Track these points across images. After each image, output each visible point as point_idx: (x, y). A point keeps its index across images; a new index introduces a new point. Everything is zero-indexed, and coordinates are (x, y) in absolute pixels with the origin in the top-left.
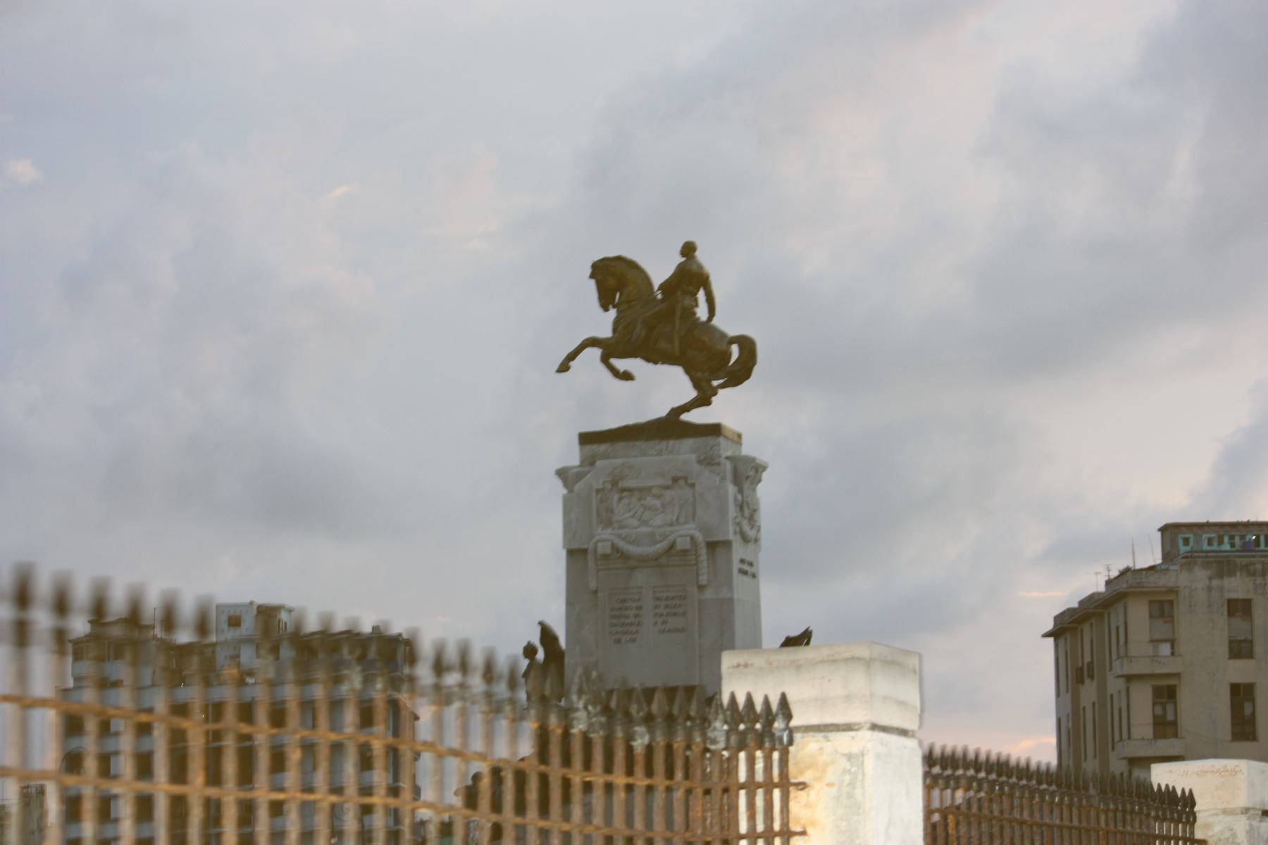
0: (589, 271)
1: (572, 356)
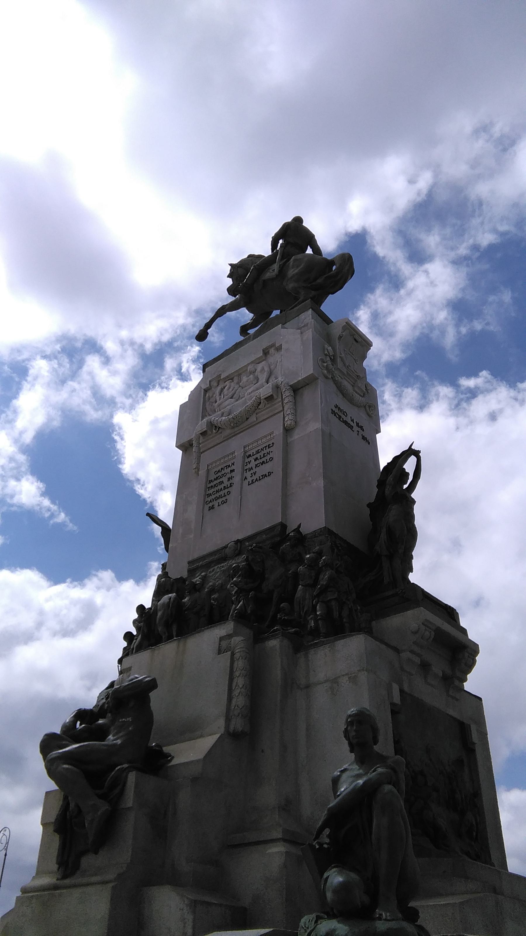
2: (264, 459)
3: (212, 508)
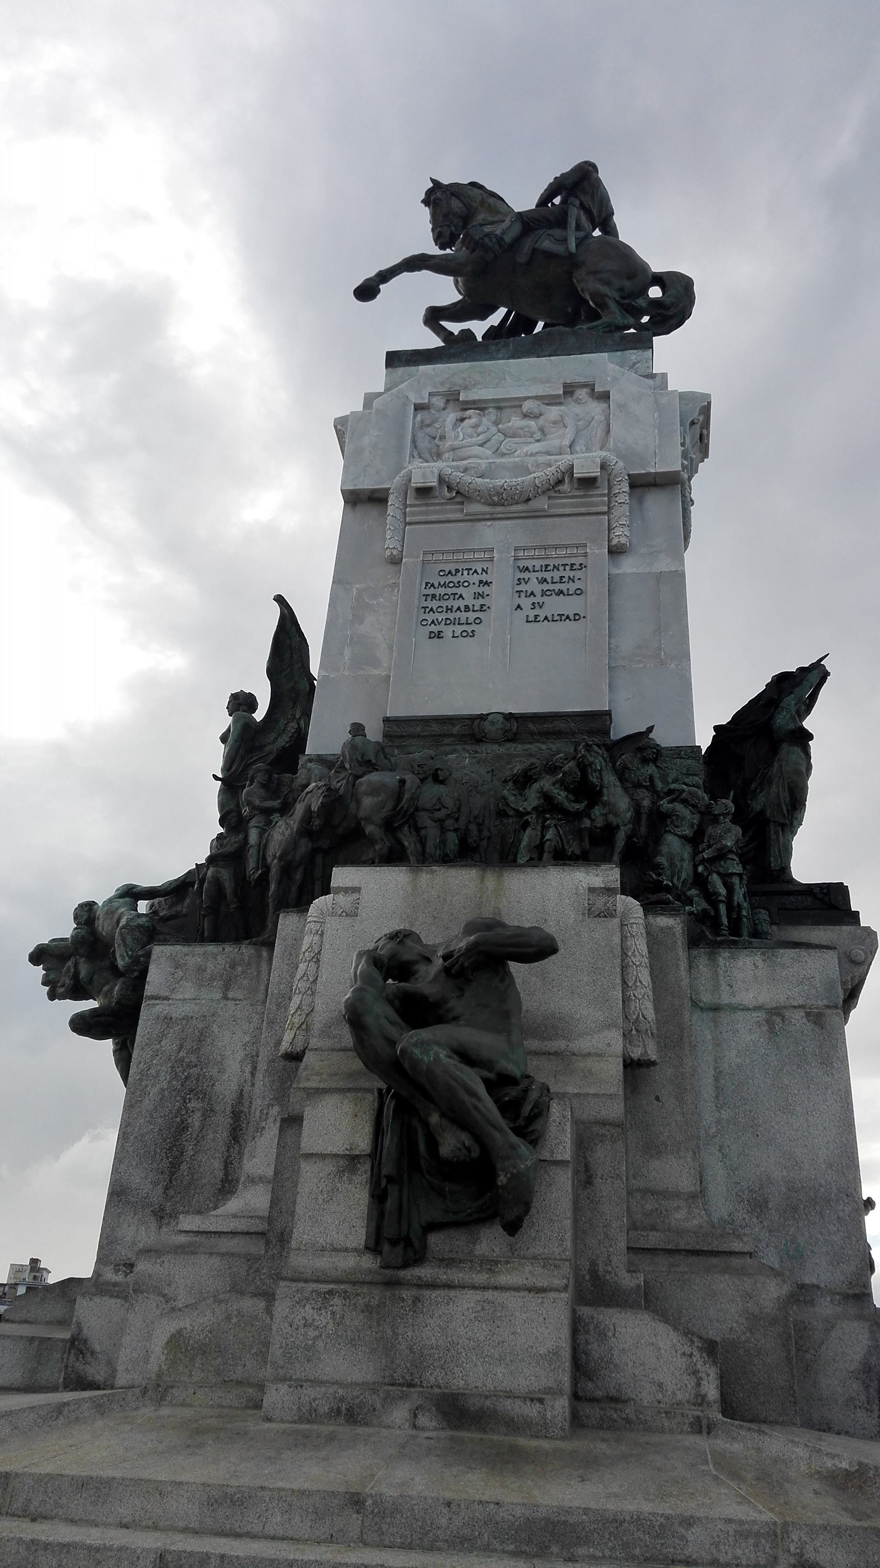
0: (349, 729)
1: (385, 276)
2: (563, 587)
3: (439, 635)
